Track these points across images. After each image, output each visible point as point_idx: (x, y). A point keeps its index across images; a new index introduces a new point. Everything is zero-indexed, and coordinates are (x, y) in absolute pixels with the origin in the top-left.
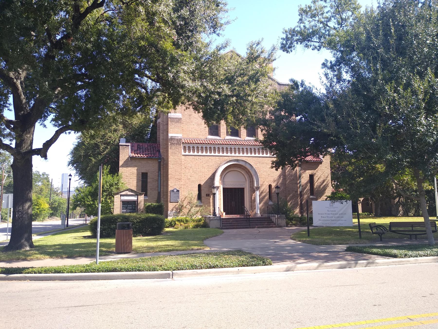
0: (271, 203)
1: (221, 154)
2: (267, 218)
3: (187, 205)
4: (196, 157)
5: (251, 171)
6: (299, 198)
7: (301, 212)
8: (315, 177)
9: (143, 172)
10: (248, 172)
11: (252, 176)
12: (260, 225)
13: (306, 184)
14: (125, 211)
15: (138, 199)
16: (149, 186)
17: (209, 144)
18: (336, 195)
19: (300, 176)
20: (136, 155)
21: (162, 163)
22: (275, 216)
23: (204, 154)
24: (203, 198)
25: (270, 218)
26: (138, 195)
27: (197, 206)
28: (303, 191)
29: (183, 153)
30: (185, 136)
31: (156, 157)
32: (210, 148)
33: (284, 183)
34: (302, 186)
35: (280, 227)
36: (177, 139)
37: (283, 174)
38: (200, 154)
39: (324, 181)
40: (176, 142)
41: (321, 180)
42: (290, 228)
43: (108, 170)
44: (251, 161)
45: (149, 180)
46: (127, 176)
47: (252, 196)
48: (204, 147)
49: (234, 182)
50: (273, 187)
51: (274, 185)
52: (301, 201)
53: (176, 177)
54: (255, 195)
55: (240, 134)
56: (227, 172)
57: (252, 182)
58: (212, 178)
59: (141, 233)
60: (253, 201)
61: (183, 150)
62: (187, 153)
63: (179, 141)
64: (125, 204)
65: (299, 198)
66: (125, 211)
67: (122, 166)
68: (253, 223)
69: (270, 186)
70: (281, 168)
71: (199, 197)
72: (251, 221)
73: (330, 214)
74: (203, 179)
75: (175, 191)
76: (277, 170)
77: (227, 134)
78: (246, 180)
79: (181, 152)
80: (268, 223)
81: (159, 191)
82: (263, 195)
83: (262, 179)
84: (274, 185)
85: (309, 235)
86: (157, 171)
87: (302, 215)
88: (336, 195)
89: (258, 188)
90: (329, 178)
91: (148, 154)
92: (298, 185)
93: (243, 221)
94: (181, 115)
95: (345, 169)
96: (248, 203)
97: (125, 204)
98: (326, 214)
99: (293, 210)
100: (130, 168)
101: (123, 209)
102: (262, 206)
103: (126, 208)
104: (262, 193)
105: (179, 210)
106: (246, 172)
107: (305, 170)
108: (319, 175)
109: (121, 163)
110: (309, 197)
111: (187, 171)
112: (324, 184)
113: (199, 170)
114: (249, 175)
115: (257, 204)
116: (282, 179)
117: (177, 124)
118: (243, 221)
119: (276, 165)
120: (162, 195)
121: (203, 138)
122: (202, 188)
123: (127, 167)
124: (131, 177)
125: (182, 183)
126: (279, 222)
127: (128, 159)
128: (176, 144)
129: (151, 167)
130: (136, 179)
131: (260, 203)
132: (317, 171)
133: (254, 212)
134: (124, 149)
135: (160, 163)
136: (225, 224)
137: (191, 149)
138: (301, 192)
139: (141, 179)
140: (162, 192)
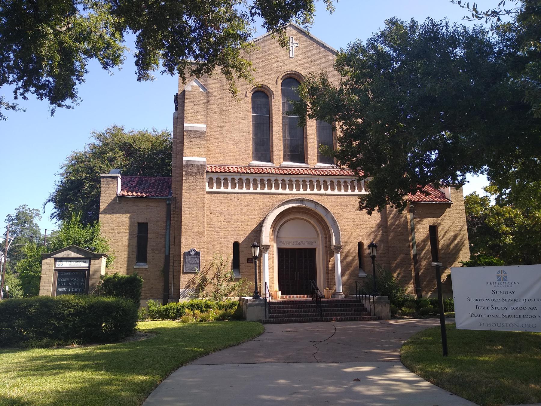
0: (362, 274)
1: (273, 190)
2: (355, 302)
3: (213, 279)
4: (229, 195)
5: (325, 218)
6: (412, 266)
7: (418, 290)
8: (439, 230)
9: (140, 221)
10: (321, 221)
11: (328, 228)
12: (341, 315)
13: (424, 241)
14: (64, 290)
15: (89, 267)
16: (151, 245)
17: (252, 173)
18: (480, 260)
19: (413, 229)
20: (130, 194)
21: (173, 207)
22: (369, 299)
23: (244, 190)
24: (241, 266)
25: (360, 301)
26: (90, 259)
27: (230, 280)
28: (420, 254)
29: (208, 189)
30: (213, 161)
31: (162, 196)
32: (255, 180)
33: (384, 239)
34: (418, 245)
35: (380, 319)
36: (198, 166)
37: (383, 225)
38: (237, 190)
39: (455, 237)
40: (194, 170)
41: (450, 235)
42: (400, 322)
43: (78, 218)
44: (326, 202)
45: (149, 236)
46: (112, 229)
47: (328, 262)
48: (244, 178)
49: (298, 237)
50: (366, 245)
51: (366, 242)
52: (417, 271)
53: (194, 230)
54: (333, 260)
55: (307, 158)
56: (284, 220)
57: (328, 238)
58: (258, 231)
59: (78, 337)
60: (330, 272)
61: (207, 184)
62: (215, 189)
63: (200, 169)
64: (63, 275)
65: (412, 266)
66: (64, 290)
67: (105, 212)
68: (328, 311)
69: (360, 245)
70: (376, 208)
71: (236, 264)
72: (325, 306)
73: (498, 300)
74: (242, 232)
75: (193, 253)
76: (369, 213)
77: (285, 160)
78: (318, 235)
79: (205, 186)
80: (357, 310)
81: (167, 254)
82: (350, 259)
83: (346, 233)
84: (366, 242)
85: (445, 353)
86: (165, 220)
87: (420, 297)
88: (480, 260)
89: (338, 248)
90: (465, 232)
91: (152, 192)
92: (411, 244)
93: (309, 307)
94: (205, 126)
95: (483, 222)
96: (322, 274)
97: (63, 275)
98: (488, 299)
99: (403, 286)
100: (118, 215)
101: (59, 287)
102: (348, 280)
103: (67, 285)
104: (347, 256)
105: (200, 287)
106: (318, 221)
107: (422, 217)
108: (447, 227)
109: (102, 207)
110: (429, 264)
111: (214, 219)
112: (456, 242)
113: (235, 217)
114: (322, 225)
115: (337, 276)
116: (381, 233)
117: (198, 141)
118: (309, 307)
119: (368, 204)
120: (171, 261)
121: (243, 164)
122: (241, 249)
123: (113, 213)
124: (119, 231)
125: (205, 240)
126: (377, 310)
127: (114, 200)
128: (196, 173)
129: (154, 214)
130: (127, 234)
131: (343, 274)
132: (443, 220)
133: (333, 291)
134: (108, 183)
135: (169, 205)
136: (276, 313)
137: (222, 181)
138: (415, 256)
139: (136, 233)
140: (171, 255)
